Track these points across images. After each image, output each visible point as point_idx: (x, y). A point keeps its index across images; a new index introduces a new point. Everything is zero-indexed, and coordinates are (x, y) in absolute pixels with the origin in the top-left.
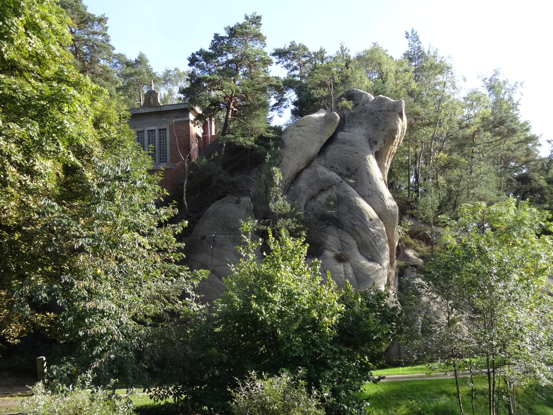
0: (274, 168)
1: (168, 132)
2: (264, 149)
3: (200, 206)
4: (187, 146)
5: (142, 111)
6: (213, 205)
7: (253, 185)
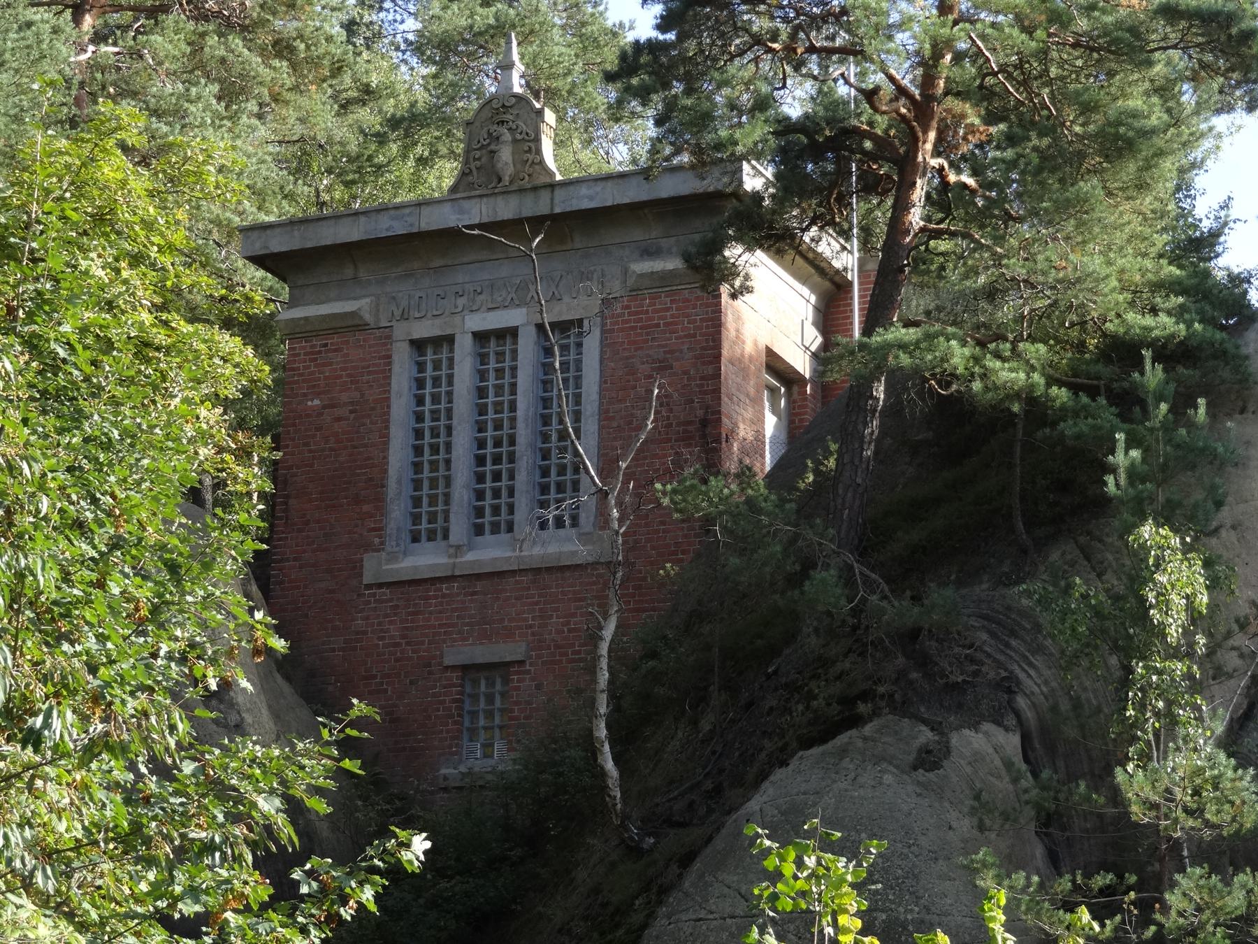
0: (1147, 531)
1: (592, 345)
2: (1106, 413)
3: (709, 785)
4: (704, 423)
5: (448, 218)
6: (779, 774)
7: (1039, 650)
